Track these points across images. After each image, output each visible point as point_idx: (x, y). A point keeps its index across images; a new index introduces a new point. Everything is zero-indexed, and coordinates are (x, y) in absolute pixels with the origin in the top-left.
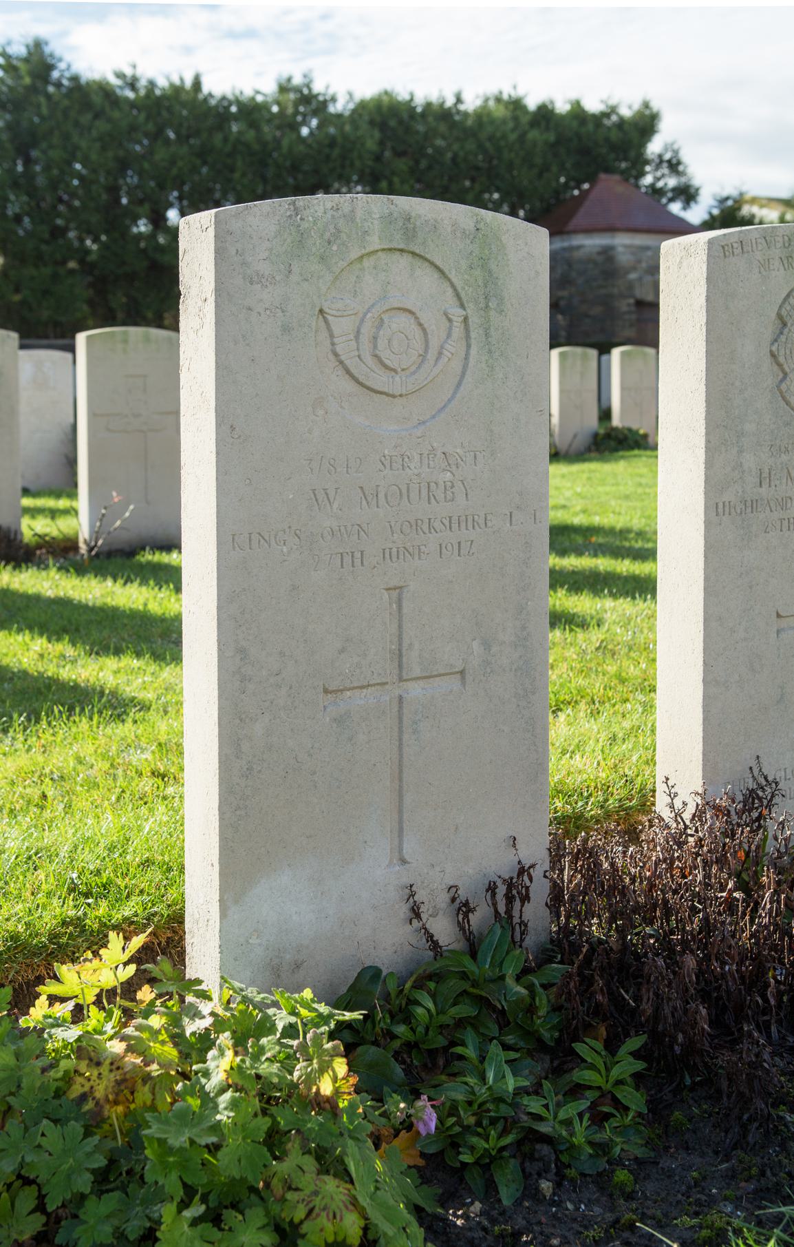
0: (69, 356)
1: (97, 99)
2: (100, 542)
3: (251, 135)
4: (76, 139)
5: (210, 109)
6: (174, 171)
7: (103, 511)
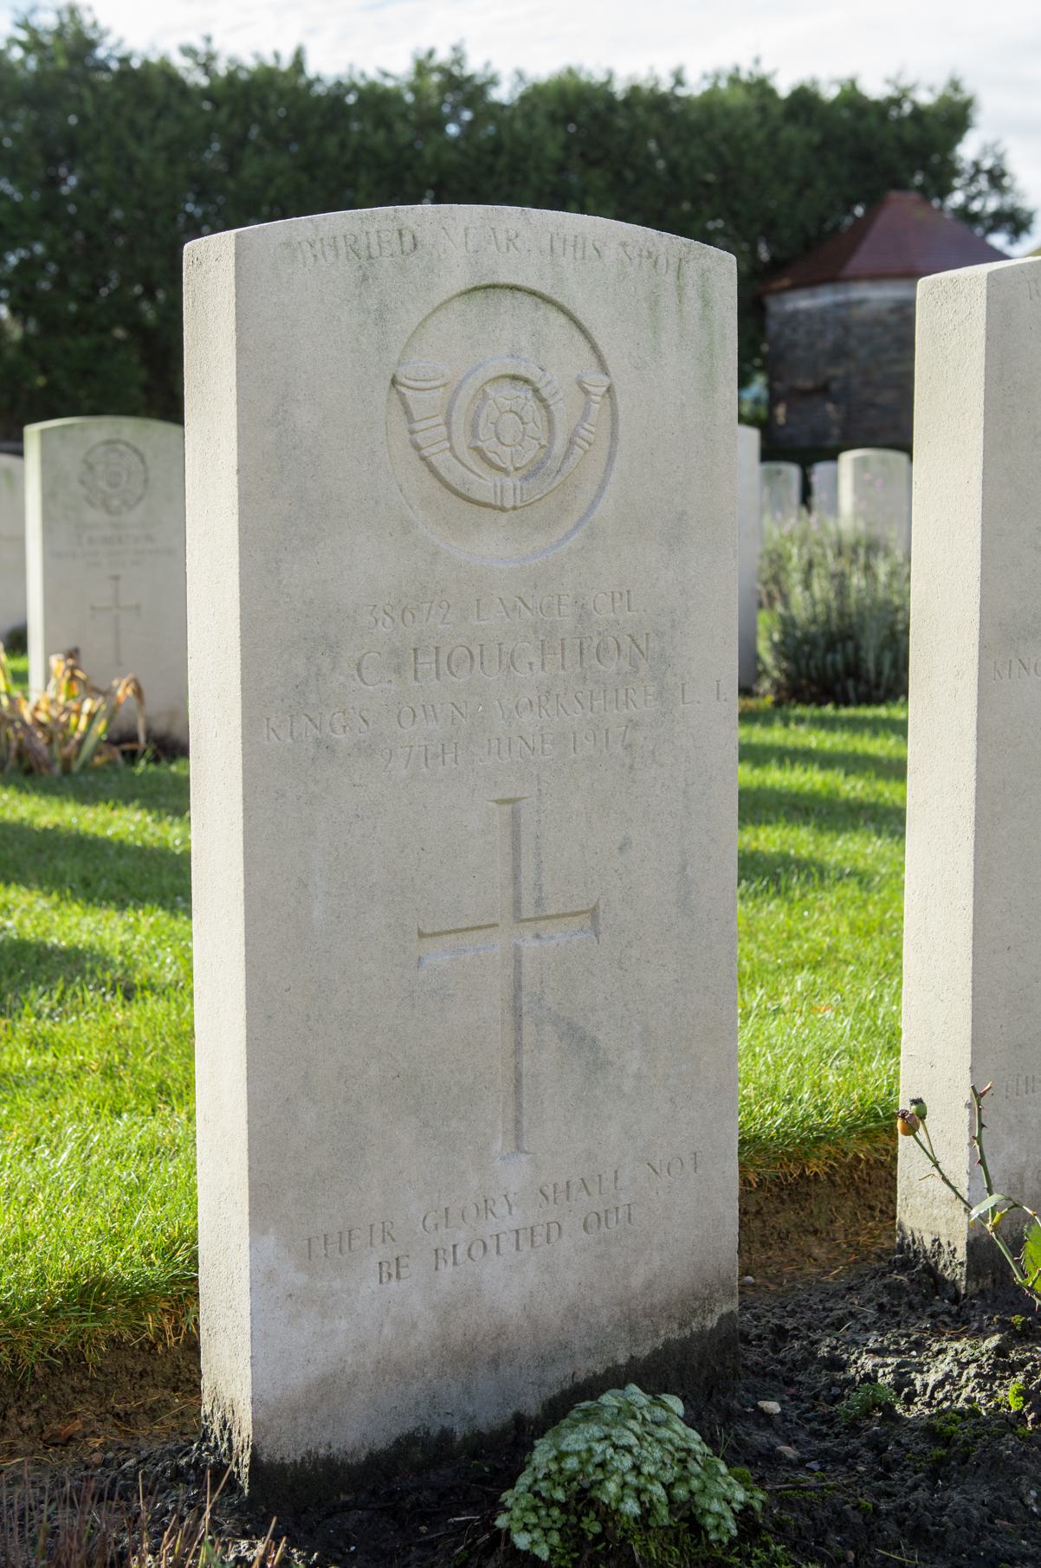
1: (159, 89)
4: (132, 146)
6: (271, 193)
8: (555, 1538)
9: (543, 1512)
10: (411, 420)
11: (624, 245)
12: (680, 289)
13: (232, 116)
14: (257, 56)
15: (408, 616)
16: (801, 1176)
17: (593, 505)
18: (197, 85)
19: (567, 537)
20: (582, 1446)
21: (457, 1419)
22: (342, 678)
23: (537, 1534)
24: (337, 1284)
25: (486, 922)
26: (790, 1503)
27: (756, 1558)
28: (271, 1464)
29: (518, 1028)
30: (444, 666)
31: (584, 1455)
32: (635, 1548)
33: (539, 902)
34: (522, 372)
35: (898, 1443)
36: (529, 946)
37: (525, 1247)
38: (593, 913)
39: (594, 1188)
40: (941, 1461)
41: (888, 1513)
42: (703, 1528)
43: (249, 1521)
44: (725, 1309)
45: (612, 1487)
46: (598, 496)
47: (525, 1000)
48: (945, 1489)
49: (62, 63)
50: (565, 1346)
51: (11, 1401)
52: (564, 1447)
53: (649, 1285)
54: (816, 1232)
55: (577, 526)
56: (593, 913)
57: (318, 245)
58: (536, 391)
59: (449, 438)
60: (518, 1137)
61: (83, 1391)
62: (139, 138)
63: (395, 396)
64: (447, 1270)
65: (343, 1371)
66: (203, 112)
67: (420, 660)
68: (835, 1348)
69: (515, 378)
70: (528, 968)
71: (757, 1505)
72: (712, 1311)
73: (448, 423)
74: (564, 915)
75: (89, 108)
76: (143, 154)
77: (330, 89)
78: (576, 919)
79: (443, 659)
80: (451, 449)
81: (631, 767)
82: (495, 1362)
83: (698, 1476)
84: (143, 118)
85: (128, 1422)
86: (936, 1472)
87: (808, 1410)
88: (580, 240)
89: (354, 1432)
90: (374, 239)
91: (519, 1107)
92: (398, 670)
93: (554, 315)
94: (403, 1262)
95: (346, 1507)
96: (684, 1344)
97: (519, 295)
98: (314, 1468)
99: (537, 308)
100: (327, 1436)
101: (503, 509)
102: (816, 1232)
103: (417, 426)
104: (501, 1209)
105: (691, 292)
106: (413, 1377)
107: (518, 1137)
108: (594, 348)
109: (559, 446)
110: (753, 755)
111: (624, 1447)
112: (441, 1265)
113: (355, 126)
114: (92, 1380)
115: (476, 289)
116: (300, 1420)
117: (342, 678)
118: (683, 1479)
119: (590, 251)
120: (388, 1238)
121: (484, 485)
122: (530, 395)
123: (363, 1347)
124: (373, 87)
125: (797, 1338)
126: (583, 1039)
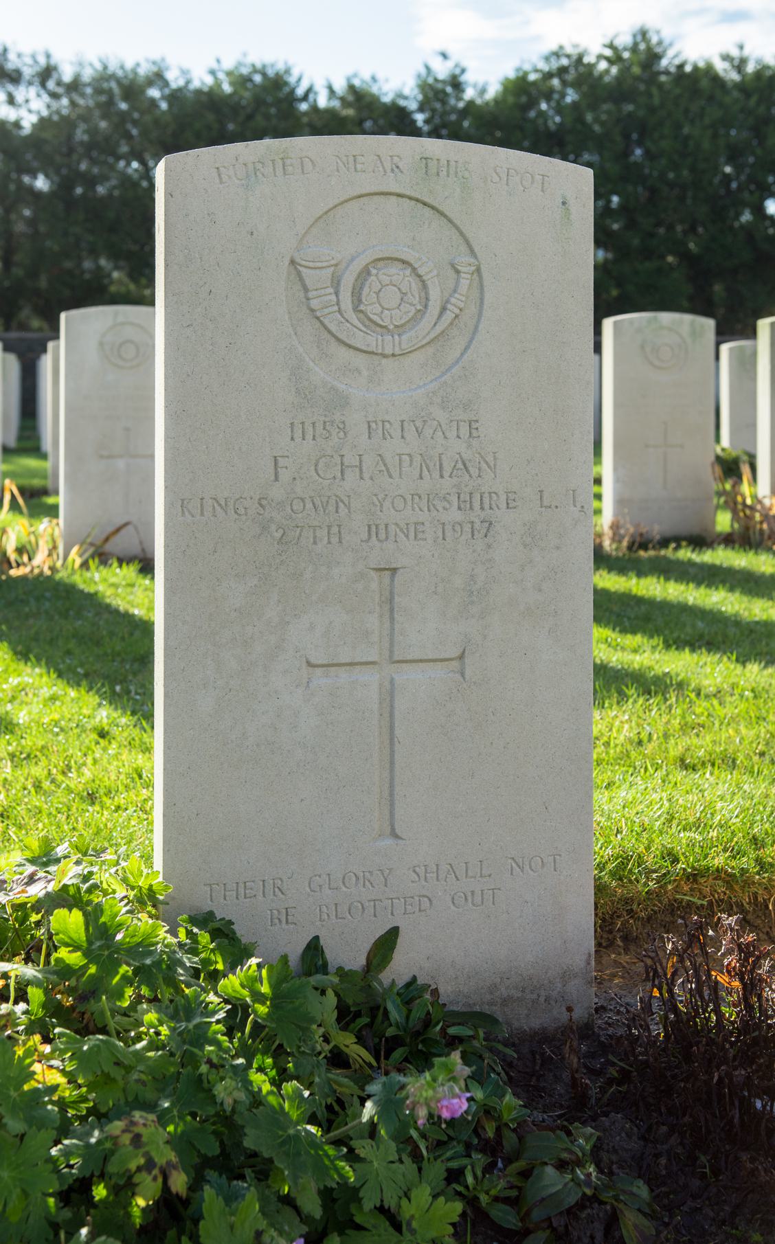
1: (704, 83)
49: (636, 70)
59: (338, 304)
75: (656, 101)
80: (339, 311)
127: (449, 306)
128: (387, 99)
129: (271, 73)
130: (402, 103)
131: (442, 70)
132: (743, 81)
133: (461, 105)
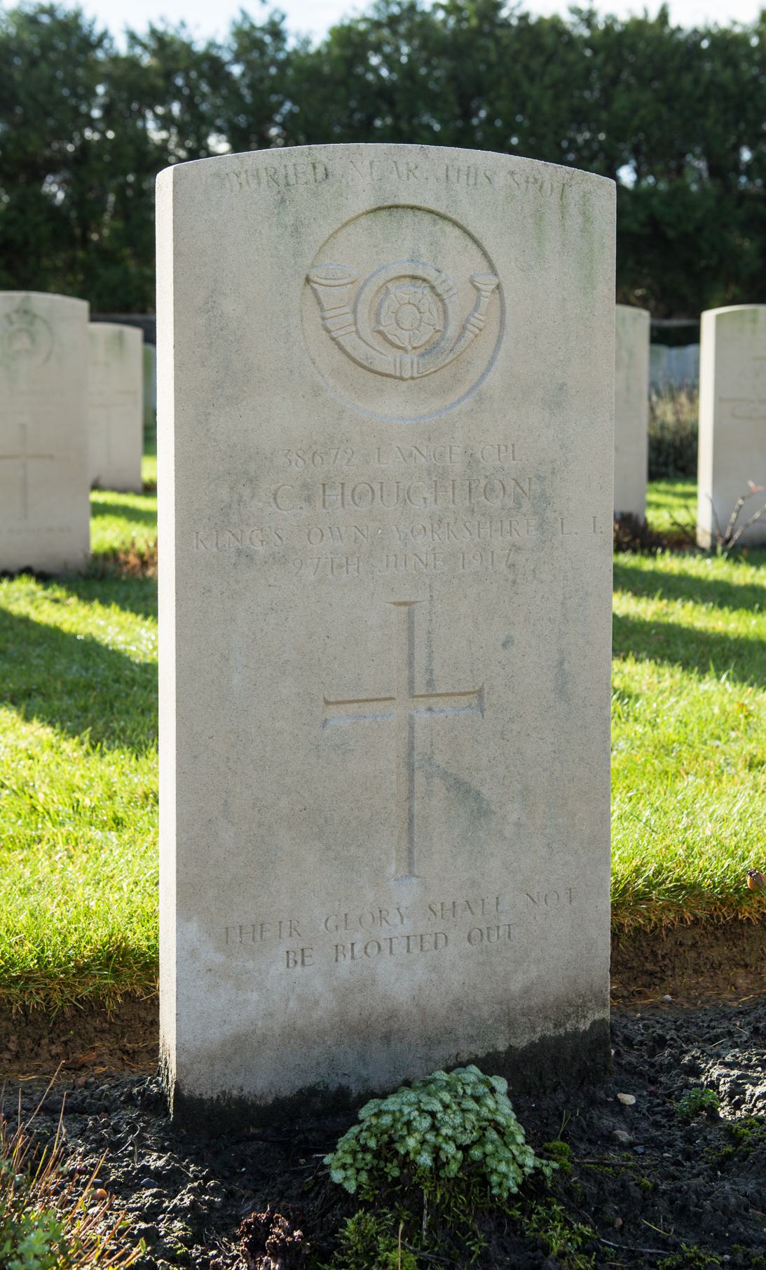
0: (134, 335)
1: (549, 40)
2: (736, 536)
3: (726, 75)
4: (525, 85)
5: (679, 44)
6: (636, 122)
7: (740, 502)
8: (364, 1177)
9: (360, 1156)
10: (322, 309)
11: (512, 173)
12: (563, 208)
13: (606, 61)
14: (630, 11)
15: (318, 459)
16: (735, 919)
17: (483, 376)
18: (581, 36)
19: (459, 401)
20: (395, 1107)
21: (353, 1079)
22: (260, 505)
23: (351, 1172)
24: (250, 965)
25: (383, 696)
26: (588, 1174)
27: (538, 1213)
28: (191, 1098)
29: (411, 780)
30: (348, 497)
31: (398, 1114)
32: (426, 1192)
33: (430, 683)
34: (419, 273)
35: (705, 1138)
36: (422, 717)
37: (415, 951)
38: (480, 693)
39: (478, 911)
40: (728, 1156)
41: (664, 1192)
42: (489, 1183)
43: (170, 1140)
44: (597, 1016)
45: (412, 1142)
46: (488, 370)
47: (416, 758)
48: (723, 1179)
50: (450, 1032)
51: (45, 1033)
52: (383, 1107)
53: (526, 991)
54: (746, 966)
55: (468, 393)
56: (480, 693)
57: (243, 176)
58: (433, 288)
59: (355, 323)
60: (410, 865)
61: (103, 1031)
62: (532, 79)
63: (309, 291)
64: (345, 962)
65: (254, 1032)
66: (584, 57)
67: (328, 493)
68: (698, 1058)
69: (414, 278)
70: (419, 733)
71: (547, 1171)
72: (585, 1017)
73: (354, 312)
74: (453, 694)
75: (493, 56)
76: (535, 92)
77: (689, 36)
78: (465, 698)
79: (348, 493)
80: (357, 332)
81: (514, 582)
82: (387, 1038)
83: (493, 1142)
84: (536, 64)
85: (133, 1059)
86: (723, 1164)
87: (658, 1105)
88: (472, 170)
89: (264, 1081)
90: (291, 171)
91: (411, 840)
92: (309, 499)
93: (449, 228)
94: (307, 953)
95: (253, 1138)
96: (558, 1040)
97: (418, 213)
98: (228, 1105)
99: (435, 224)
100: (239, 1081)
101: (402, 379)
102: (746, 966)
103: (327, 315)
104: (394, 918)
105: (573, 210)
106: (315, 1042)
107: (410, 865)
108: (485, 254)
109: (452, 331)
110: (627, 581)
111: (428, 1112)
112: (341, 958)
113: (708, 66)
114: (111, 1023)
115: (380, 209)
116: (216, 1067)
117: (260, 505)
118: (480, 1141)
119: (482, 179)
120: (294, 933)
121: (385, 360)
122: (427, 291)
123: (271, 1015)
124: (725, 33)
125: (671, 1046)
126: (468, 791)
127: (469, 326)
128: (200, 47)
129: (60, 15)
130: (214, 52)
131: (260, 17)
132: (592, 37)
133: (282, 56)
